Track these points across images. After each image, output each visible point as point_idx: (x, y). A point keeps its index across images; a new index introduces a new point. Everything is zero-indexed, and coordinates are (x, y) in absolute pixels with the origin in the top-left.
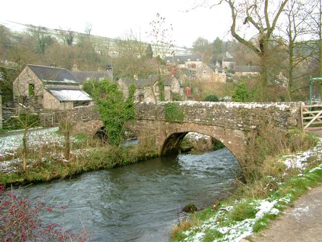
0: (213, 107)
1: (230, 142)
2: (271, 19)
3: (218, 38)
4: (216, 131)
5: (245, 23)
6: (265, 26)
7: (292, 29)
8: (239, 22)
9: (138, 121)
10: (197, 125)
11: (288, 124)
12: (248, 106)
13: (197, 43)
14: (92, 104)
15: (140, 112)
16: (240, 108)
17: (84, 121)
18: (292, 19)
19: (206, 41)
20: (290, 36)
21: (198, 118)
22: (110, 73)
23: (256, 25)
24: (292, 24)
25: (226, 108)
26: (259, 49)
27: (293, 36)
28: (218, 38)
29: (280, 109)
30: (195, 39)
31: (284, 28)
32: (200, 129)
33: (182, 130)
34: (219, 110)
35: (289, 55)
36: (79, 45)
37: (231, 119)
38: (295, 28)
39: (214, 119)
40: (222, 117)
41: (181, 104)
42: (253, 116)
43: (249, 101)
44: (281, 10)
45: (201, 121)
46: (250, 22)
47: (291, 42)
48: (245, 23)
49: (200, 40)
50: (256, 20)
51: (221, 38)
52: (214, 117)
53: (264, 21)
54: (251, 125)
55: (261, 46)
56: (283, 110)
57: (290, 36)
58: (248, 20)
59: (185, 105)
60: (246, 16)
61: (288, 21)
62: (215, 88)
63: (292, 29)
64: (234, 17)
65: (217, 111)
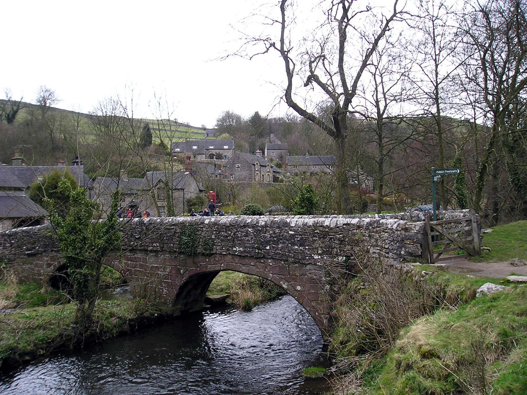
0: (266, 226)
1: (299, 288)
2: (351, 74)
3: (257, 114)
4: (273, 268)
5: (306, 85)
6: (340, 90)
7: (380, 96)
8: (298, 81)
9: (128, 254)
10: (237, 260)
11: (405, 252)
12: (328, 221)
13: (223, 120)
14: (47, 223)
15: (132, 235)
16: (316, 225)
17: (28, 255)
18: (379, 80)
19: (238, 118)
20: (377, 106)
21: (240, 245)
22: (79, 169)
23: (323, 86)
24: (380, 89)
25: (291, 229)
26: (333, 128)
27: (382, 108)
28: (257, 114)
29: (389, 226)
30: (220, 114)
31: (369, 95)
32: (244, 265)
33: (211, 268)
34: (277, 231)
35: (376, 137)
36: (28, 124)
37: (301, 245)
38: (384, 94)
39: (268, 248)
40: (284, 243)
41: (207, 222)
42: (339, 239)
43: (325, 212)
44: (364, 65)
45: (244, 251)
46: (314, 83)
47: (380, 115)
48: (306, 85)
49: (229, 116)
50: (324, 79)
51: (263, 114)
52: (268, 243)
53: (337, 79)
54: (337, 255)
55: (336, 122)
56: (395, 226)
57: (377, 106)
58: (312, 78)
59: (215, 224)
60: (309, 74)
61: (374, 83)
62: (133, 240)
63: (380, 96)
64: (290, 75)
65: (274, 233)
